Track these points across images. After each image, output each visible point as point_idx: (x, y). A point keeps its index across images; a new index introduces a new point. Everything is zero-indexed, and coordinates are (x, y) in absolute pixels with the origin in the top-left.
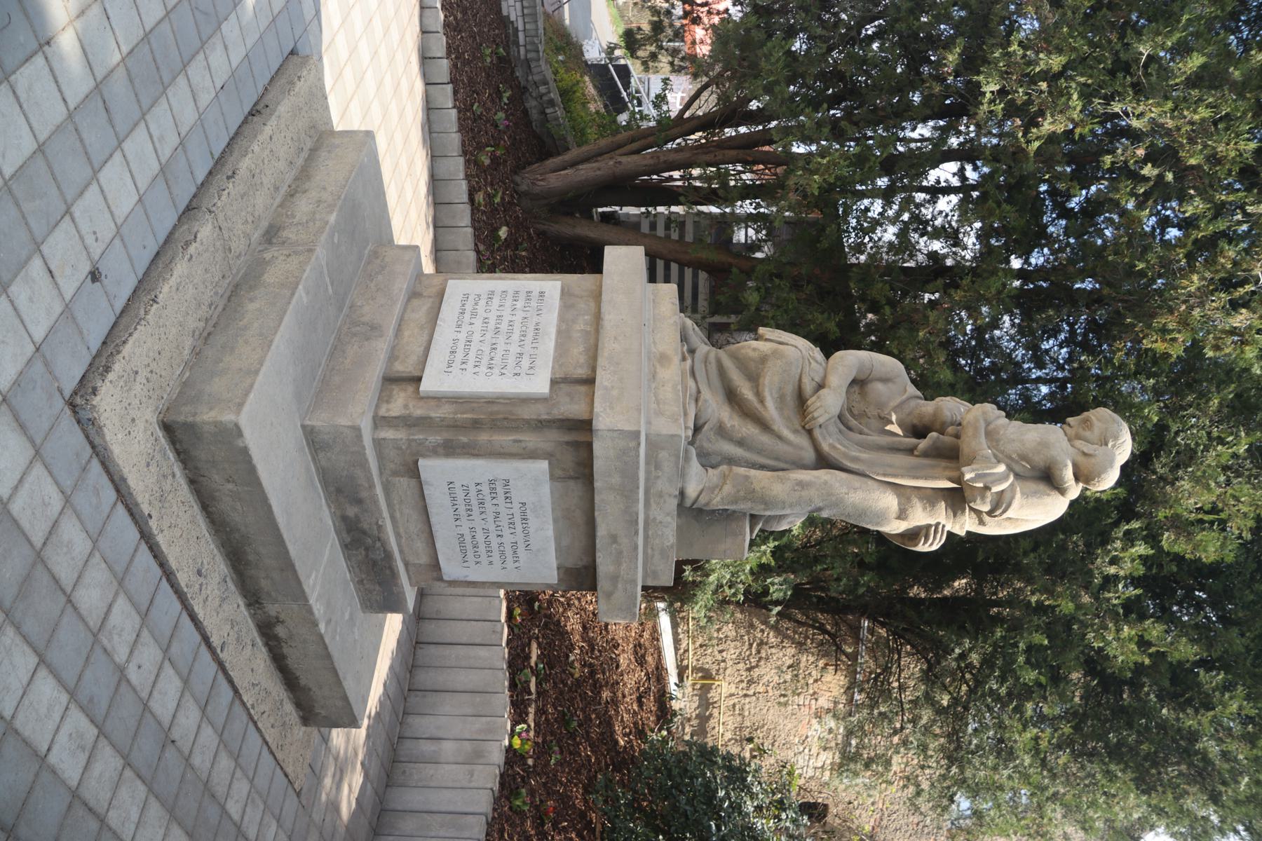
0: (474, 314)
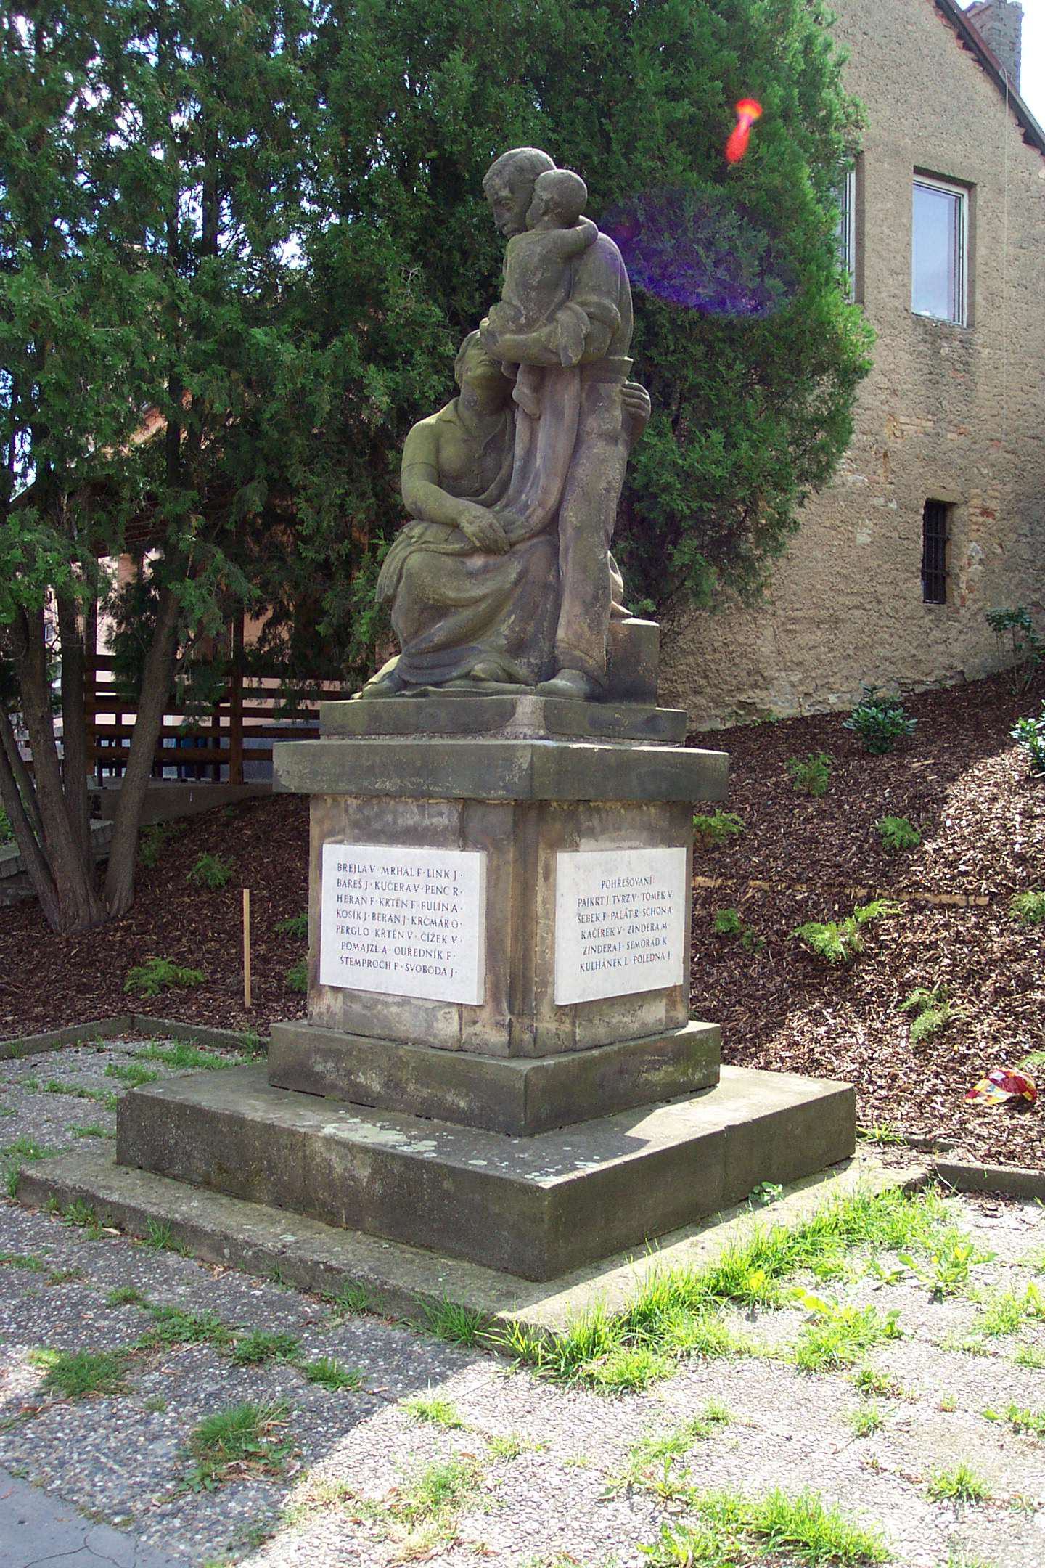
0: (373, 948)
